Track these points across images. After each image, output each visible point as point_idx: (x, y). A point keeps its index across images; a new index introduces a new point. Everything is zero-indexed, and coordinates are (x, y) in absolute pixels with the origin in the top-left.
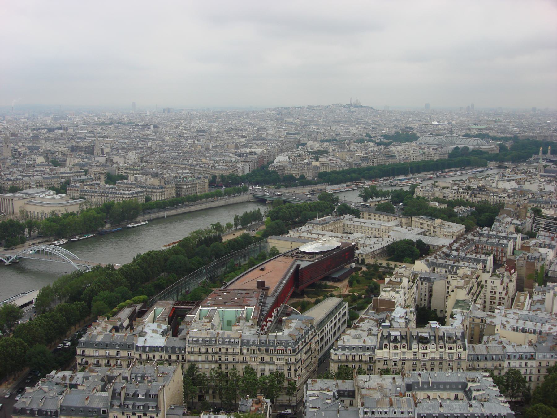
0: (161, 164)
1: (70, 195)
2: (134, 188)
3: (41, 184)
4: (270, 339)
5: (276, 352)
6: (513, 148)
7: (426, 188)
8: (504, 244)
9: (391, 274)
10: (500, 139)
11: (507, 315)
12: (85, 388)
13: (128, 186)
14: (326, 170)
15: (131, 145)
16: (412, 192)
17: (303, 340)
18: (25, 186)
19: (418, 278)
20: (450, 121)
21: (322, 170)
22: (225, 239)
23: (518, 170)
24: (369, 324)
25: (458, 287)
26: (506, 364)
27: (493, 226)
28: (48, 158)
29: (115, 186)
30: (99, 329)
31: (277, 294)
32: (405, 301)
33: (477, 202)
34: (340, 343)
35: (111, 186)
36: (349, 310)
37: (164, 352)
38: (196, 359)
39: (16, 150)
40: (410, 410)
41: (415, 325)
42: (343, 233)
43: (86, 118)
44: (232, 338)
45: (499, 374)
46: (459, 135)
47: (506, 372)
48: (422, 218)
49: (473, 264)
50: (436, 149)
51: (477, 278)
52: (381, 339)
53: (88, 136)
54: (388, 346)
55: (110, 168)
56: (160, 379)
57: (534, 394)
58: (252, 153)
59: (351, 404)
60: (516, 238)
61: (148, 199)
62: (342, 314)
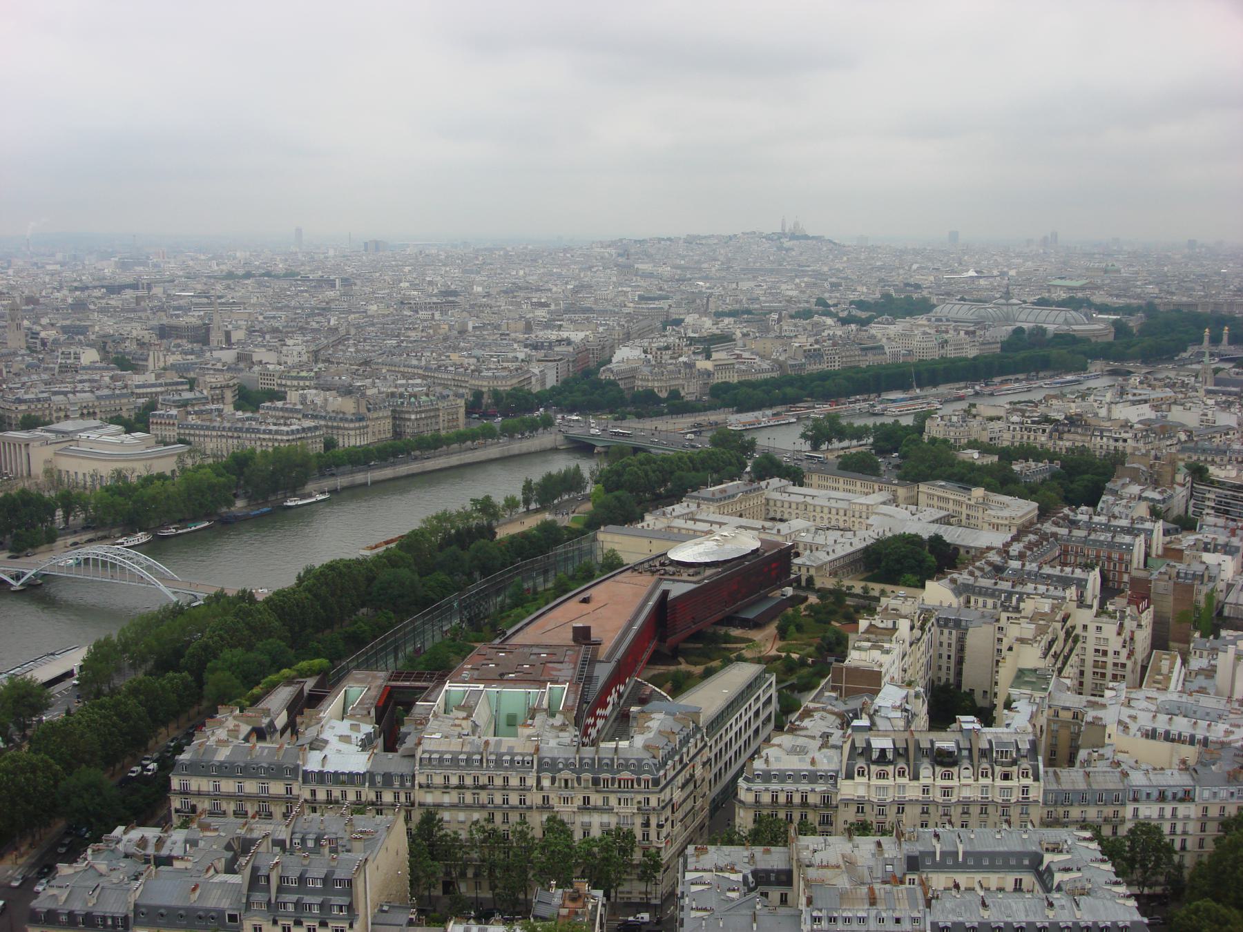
0: (360, 365)
1: (156, 435)
2: (299, 419)
3: (91, 410)
4: (603, 756)
5: (616, 785)
6: (1145, 330)
7: (950, 420)
8: (1125, 544)
9: (871, 611)
10: (1115, 310)
11: (1132, 703)
12: (189, 865)
13: (286, 415)
14: (727, 380)
15: (292, 324)
16: (920, 429)
17: (677, 758)
18: (55, 415)
19: (933, 620)
20: (1005, 269)
21: (718, 379)
22: (502, 533)
23: (1155, 379)
24: (823, 723)
25: (1022, 641)
26: (1128, 811)
27: (1100, 505)
28: (108, 352)
29: (257, 415)
30: (222, 734)
31: (619, 655)
32: (905, 671)
33: (1064, 451)
34: (758, 764)
35: (249, 415)
36: (779, 691)
37: (367, 784)
38: (438, 801)
39: (35, 335)
40: (915, 914)
41: (927, 725)
42: (766, 519)
43: (191, 263)
44: (517, 754)
45: (1115, 833)
46: (1025, 302)
47: (1130, 830)
48: (941, 486)
49: (1056, 588)
50: (974, 332)
51: (1065, 619)
52: (851, 757)
53: (196, 304)
54: (866, 772)
55: (245, 375)
56: (358, 845)
57: (1192, 879)
58: (562, 340)
59: (784, 900)
60: (1152, 531)
61: (330, 444)
62: (763, 699)
